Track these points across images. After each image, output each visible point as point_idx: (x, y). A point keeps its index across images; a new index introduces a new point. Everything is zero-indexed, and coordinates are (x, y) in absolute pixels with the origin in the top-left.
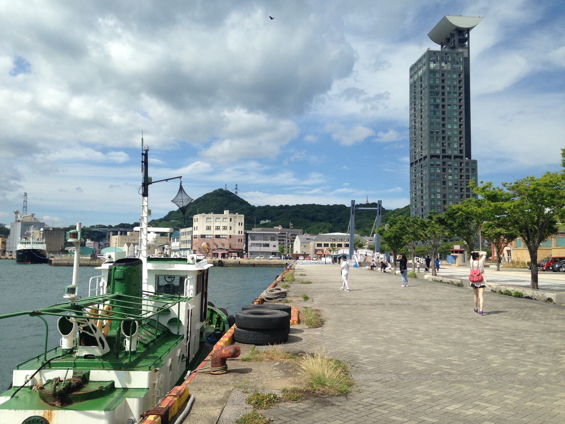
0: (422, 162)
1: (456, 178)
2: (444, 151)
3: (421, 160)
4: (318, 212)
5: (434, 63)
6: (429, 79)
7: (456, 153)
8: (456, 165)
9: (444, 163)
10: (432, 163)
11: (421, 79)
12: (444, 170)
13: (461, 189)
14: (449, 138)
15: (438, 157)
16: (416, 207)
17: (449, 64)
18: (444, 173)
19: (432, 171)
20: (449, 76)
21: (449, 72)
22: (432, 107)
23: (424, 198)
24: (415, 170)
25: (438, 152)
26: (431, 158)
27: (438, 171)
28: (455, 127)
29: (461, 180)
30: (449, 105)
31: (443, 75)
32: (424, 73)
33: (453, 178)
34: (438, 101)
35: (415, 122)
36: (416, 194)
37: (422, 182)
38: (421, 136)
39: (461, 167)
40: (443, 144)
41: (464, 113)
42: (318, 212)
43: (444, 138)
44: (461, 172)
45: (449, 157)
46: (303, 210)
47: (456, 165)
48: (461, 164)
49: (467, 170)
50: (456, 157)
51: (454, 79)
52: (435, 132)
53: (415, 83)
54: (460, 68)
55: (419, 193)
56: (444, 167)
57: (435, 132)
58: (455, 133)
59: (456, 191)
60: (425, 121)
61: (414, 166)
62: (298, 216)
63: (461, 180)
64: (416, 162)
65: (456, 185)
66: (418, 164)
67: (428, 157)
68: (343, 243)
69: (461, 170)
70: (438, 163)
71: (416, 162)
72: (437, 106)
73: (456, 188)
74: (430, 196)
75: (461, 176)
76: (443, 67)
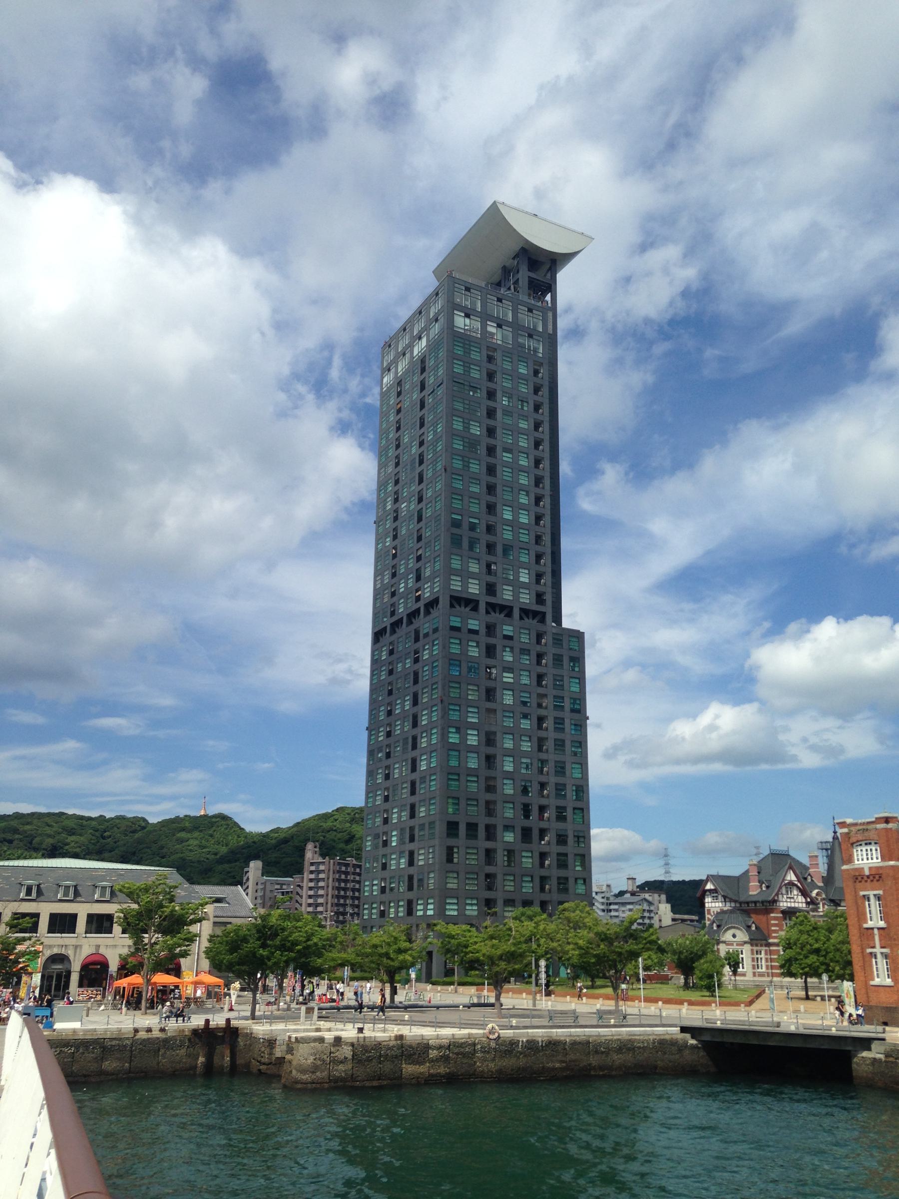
0: (418, 622)
1: (525, 680)
2: (491, 589)
3: (413, 615)
4: (71, 832)
5: (467, 316)
6: (452, 357)
7: (526, 598)
8: (525, 639)
9: (490, 629)
10: (456, 622)
11: (423, 364)
12: (490, 651)
13: (541, 720)
14: (507, 549)
15: (471, 603)
16: (387, 777)
17: (508, 332)
18: (490, 662)
19: (455, 649)
20: (508, 366)
21: (507, 353)
22: (458, 445)
23: (423, 743)
24: (391, 652)
25: (474, 589)
26: (452, 606)
27: (474, 652)
28: (524, 519)
29: (541, 690)
30: (506, 450)
31: (490, 359)
32: (433, 347)
33: (517, 678)
34: (476, 430)
35: (396, 500)
36: (389, 734)
37: (418, 688)
38: (419, 539)
39: (538, 648)
40: (488, 566)
41: (547, 482)
42: (71, 832)
43: (490, 547)
44: (539, 663)
45: (506, 610)
46: (28, 827)
47: (525, 639)
48: (539, 637)
49: (558, 660)
50: (525, 613)
51: (521, 377)
52: (465, 526)
53: (399, 384)
54: (536, 350)
55: (401, 728)
56: (492, 641)
57: (465, 526)
58: (524, 538)
59: (525, 724)
60: (435, 489)
61: (387, 638)
62: (10, 842)
63: (541, 690)
64: (396, 625)
65: (524, 703)
66: (404, 629)
67: (444, 602)
68: (82, 911)
69: (540, 656)
70: (473, 624)
71: (396, 625)
72: (472, 444)
73: (525, 716)
74: (444, 736)
75: (540, 677)
76: (492, 334)
